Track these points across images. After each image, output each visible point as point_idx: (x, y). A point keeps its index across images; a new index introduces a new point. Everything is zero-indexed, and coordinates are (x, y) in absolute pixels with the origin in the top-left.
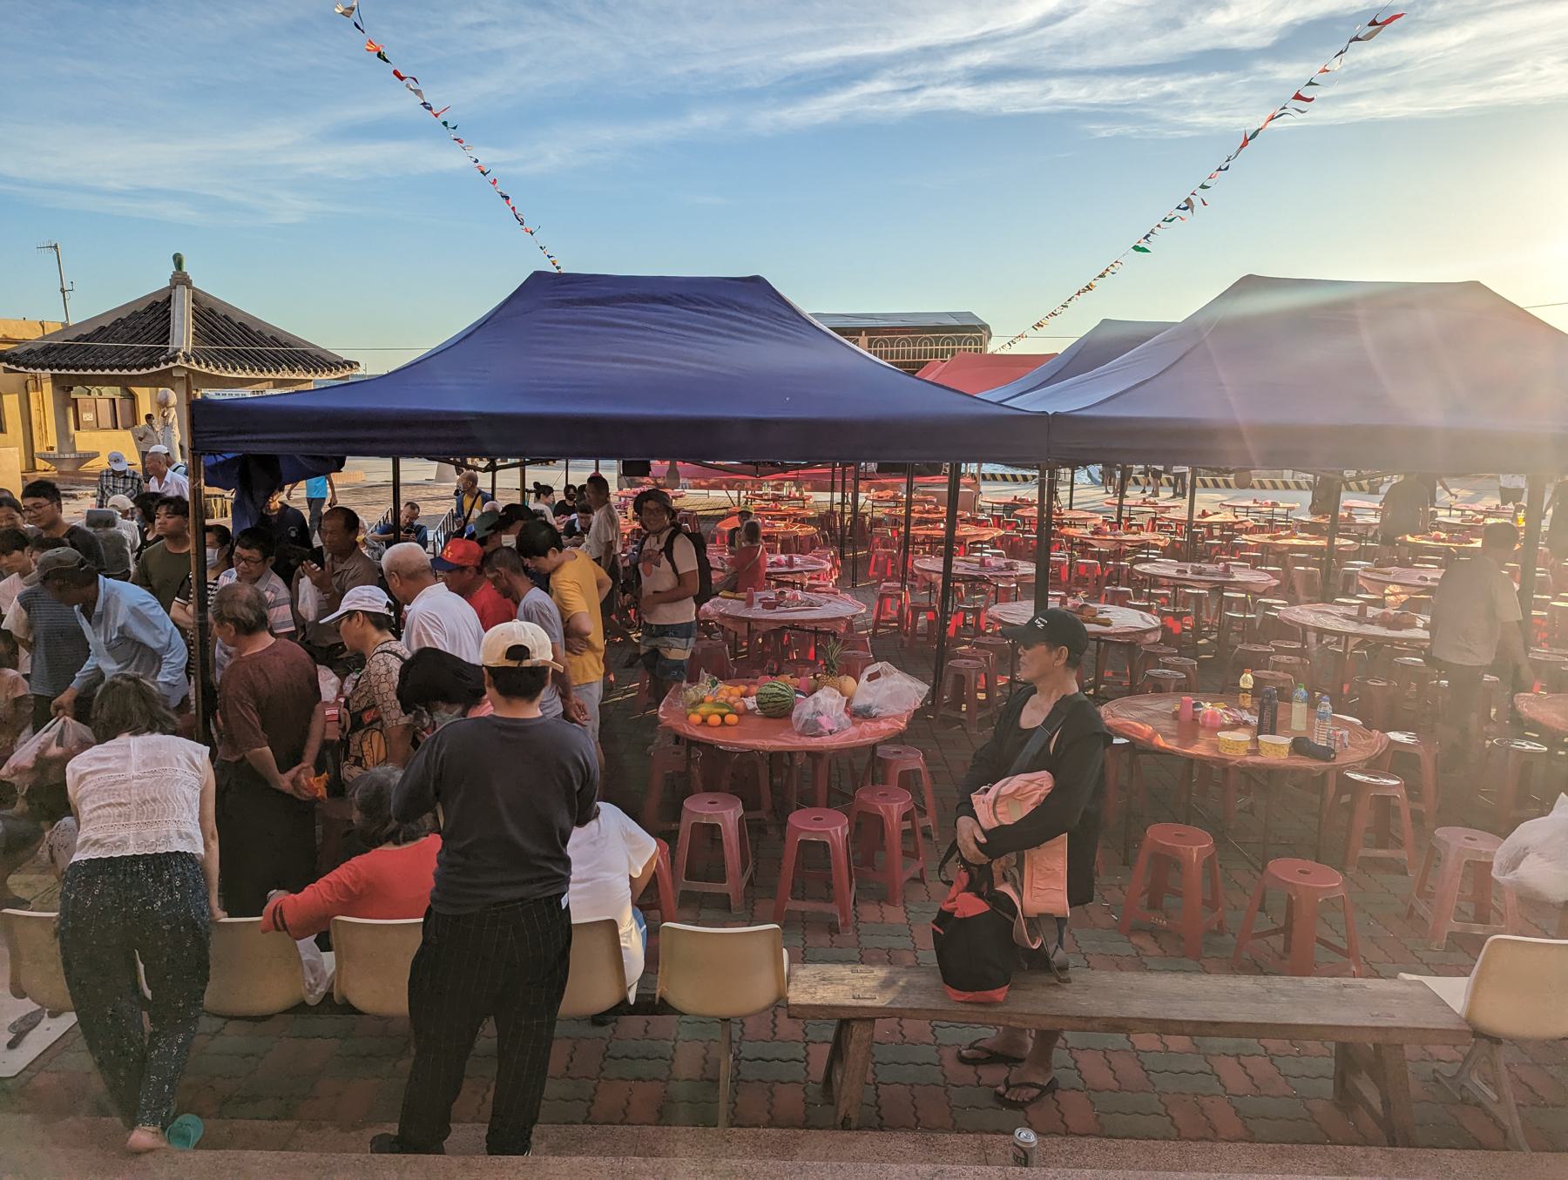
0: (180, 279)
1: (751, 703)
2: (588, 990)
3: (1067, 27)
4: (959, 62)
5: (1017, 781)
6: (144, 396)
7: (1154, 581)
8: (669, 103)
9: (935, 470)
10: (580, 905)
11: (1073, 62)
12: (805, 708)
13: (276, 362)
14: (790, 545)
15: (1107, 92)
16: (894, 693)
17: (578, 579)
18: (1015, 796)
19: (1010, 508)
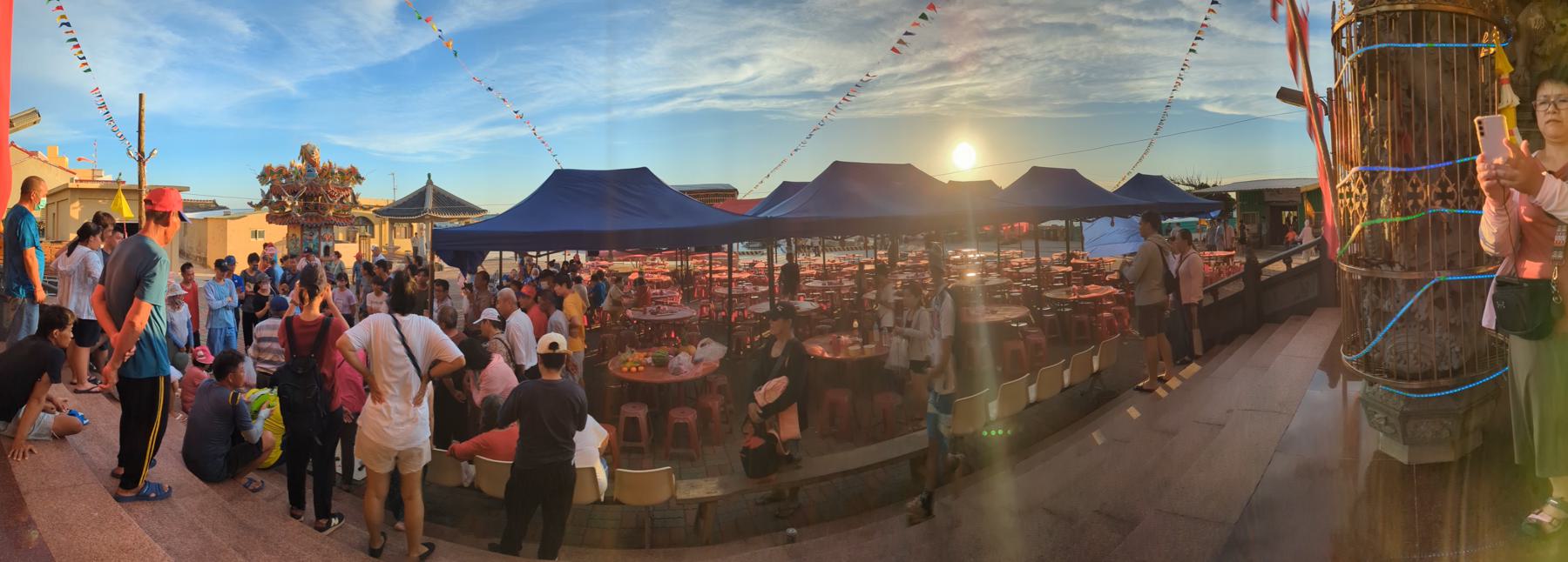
0: (430, 182)
1: (649, 360)
2: (583, 496)
3: (757, 82)
4: (716, 91)
5: (774, 382)
6: (415, 225)
7: (814, 289)
8: (608, 107)
9: (719, 249)
10: (579, 461)
11: (760, 94)
12: (674, 362)
13: (459, 212)
14: (659, 285)
15: (773, 104)
16: (712, 351)
17: (574, 303)
18: (774, 388)
19: (752, 265)
